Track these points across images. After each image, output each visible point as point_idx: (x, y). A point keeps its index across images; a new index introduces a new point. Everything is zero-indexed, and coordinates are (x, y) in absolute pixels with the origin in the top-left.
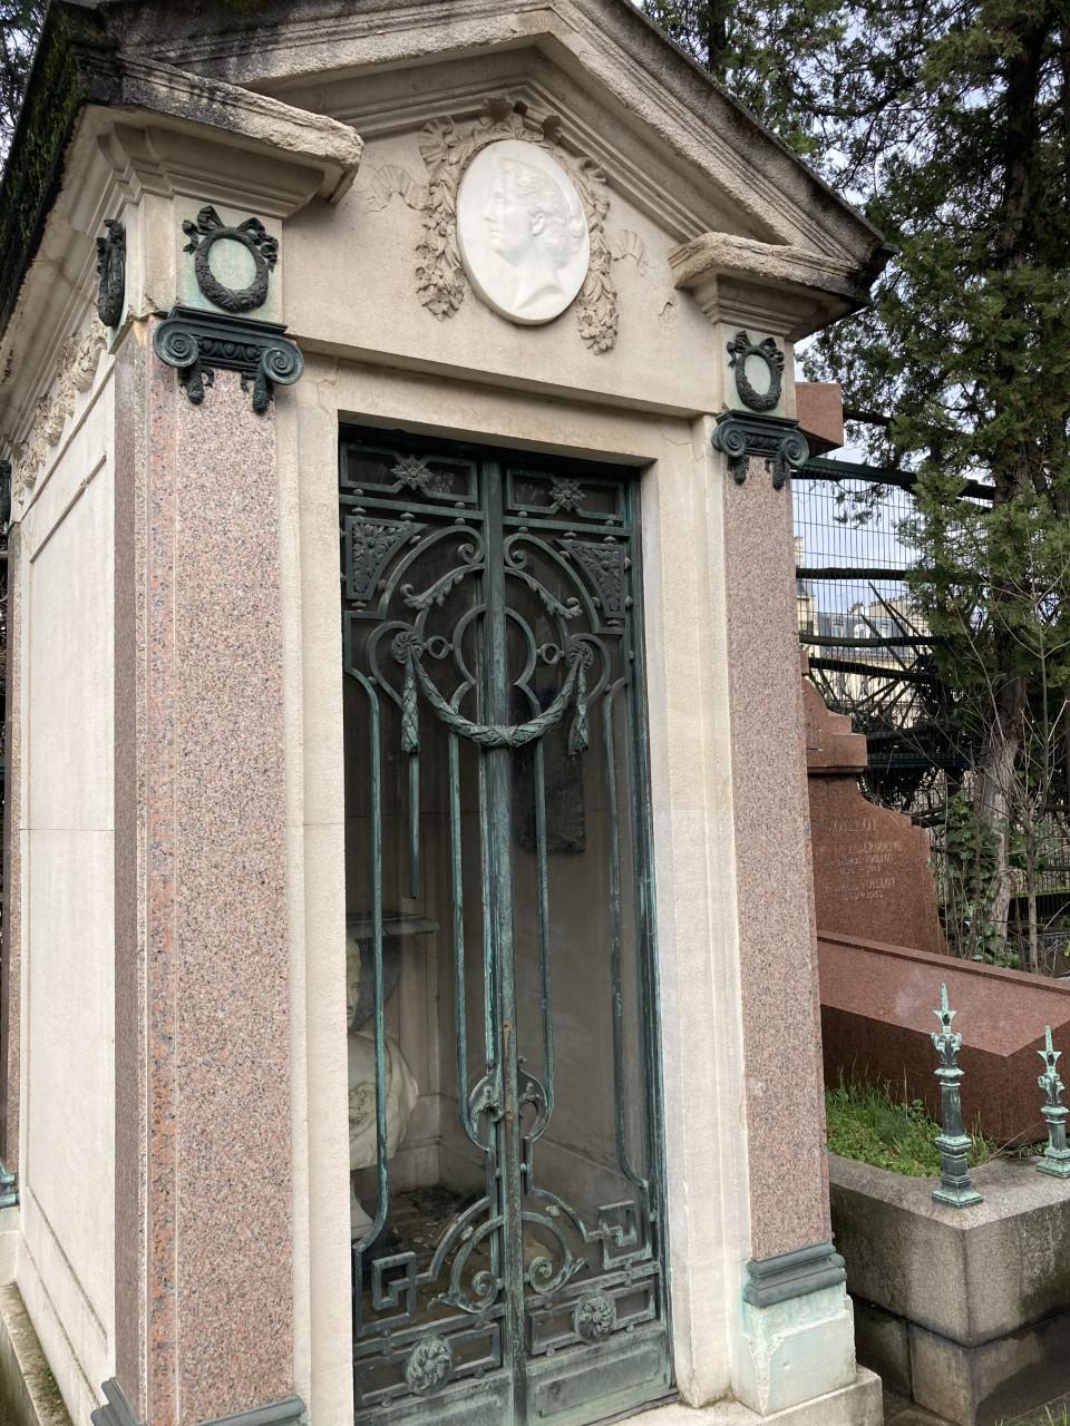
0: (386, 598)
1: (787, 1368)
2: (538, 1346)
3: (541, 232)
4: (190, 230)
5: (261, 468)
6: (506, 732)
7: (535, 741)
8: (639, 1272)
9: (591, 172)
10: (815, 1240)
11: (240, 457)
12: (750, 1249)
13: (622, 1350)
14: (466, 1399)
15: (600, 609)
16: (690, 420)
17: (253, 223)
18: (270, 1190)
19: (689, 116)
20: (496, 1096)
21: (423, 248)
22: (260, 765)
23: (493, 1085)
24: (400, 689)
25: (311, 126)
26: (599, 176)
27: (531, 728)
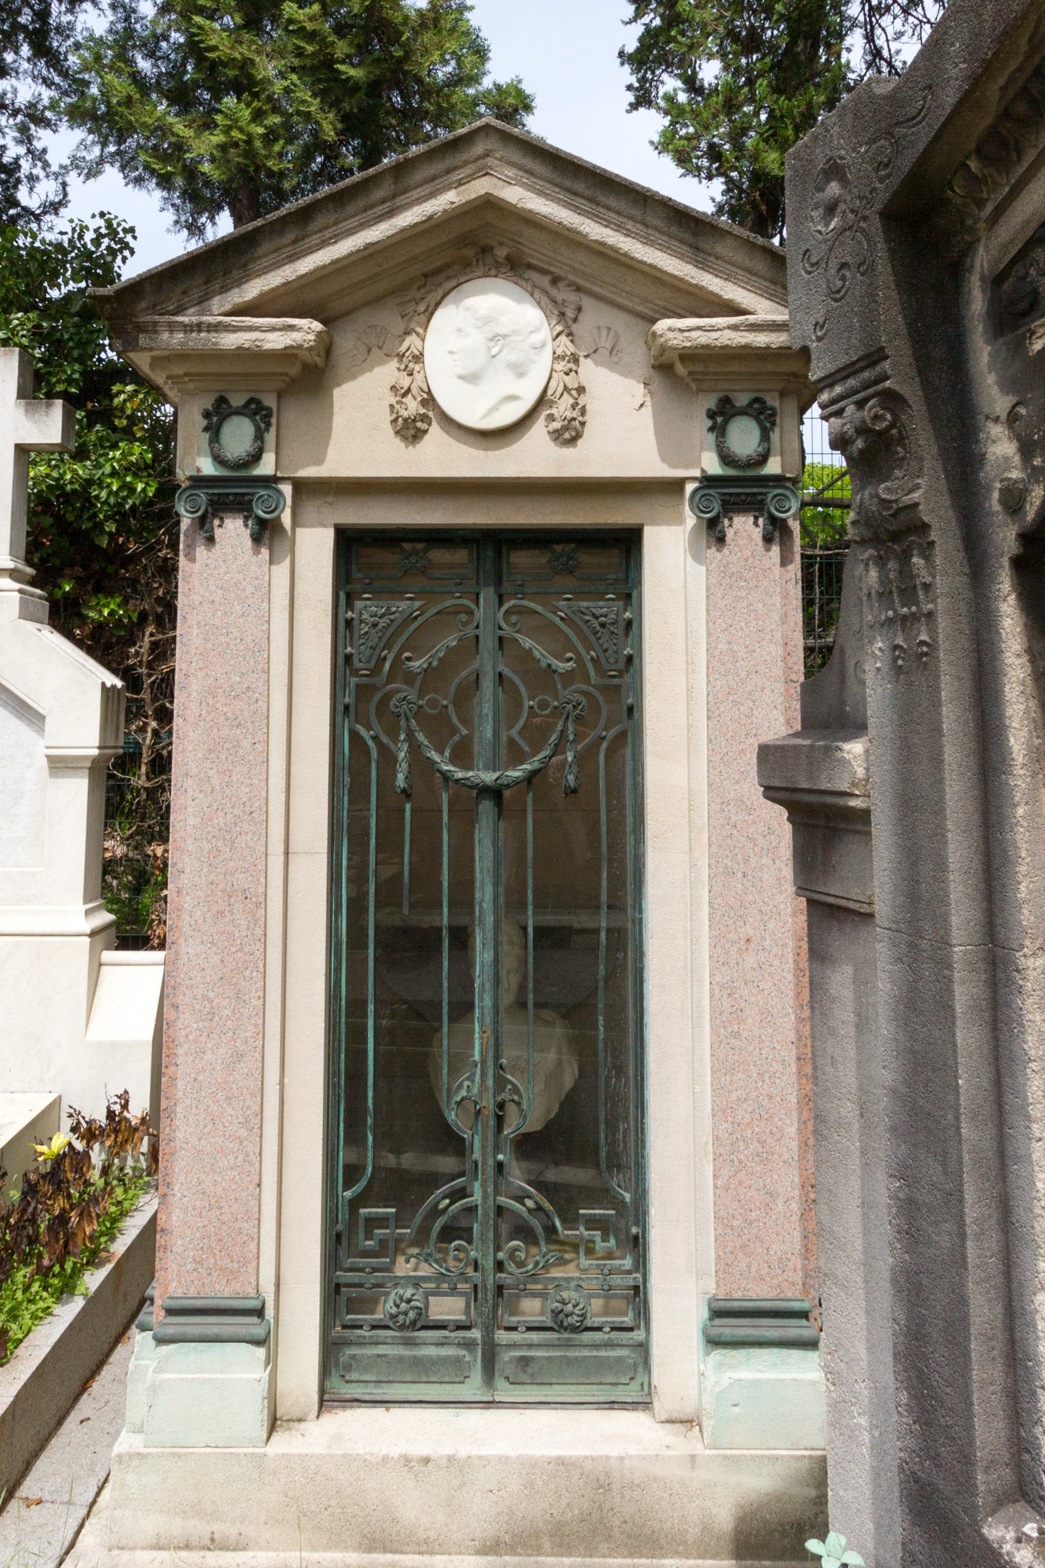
1: (736, 1409)
3: (500, 352)
4: (207, 415)
5: (256, 582)
9: (561, 285)
10: (789, 1295)
11: (241, 576)
12: (713, 1285)
13: (596, 1346)
14: (437, 1344)
16: (675, 486)
19: (630, 225)
20: (475, 1091)
22: (248, 809)
23: (473, 1081)
24: (396, 741)
25: (273, 329)
26: (569, 286)
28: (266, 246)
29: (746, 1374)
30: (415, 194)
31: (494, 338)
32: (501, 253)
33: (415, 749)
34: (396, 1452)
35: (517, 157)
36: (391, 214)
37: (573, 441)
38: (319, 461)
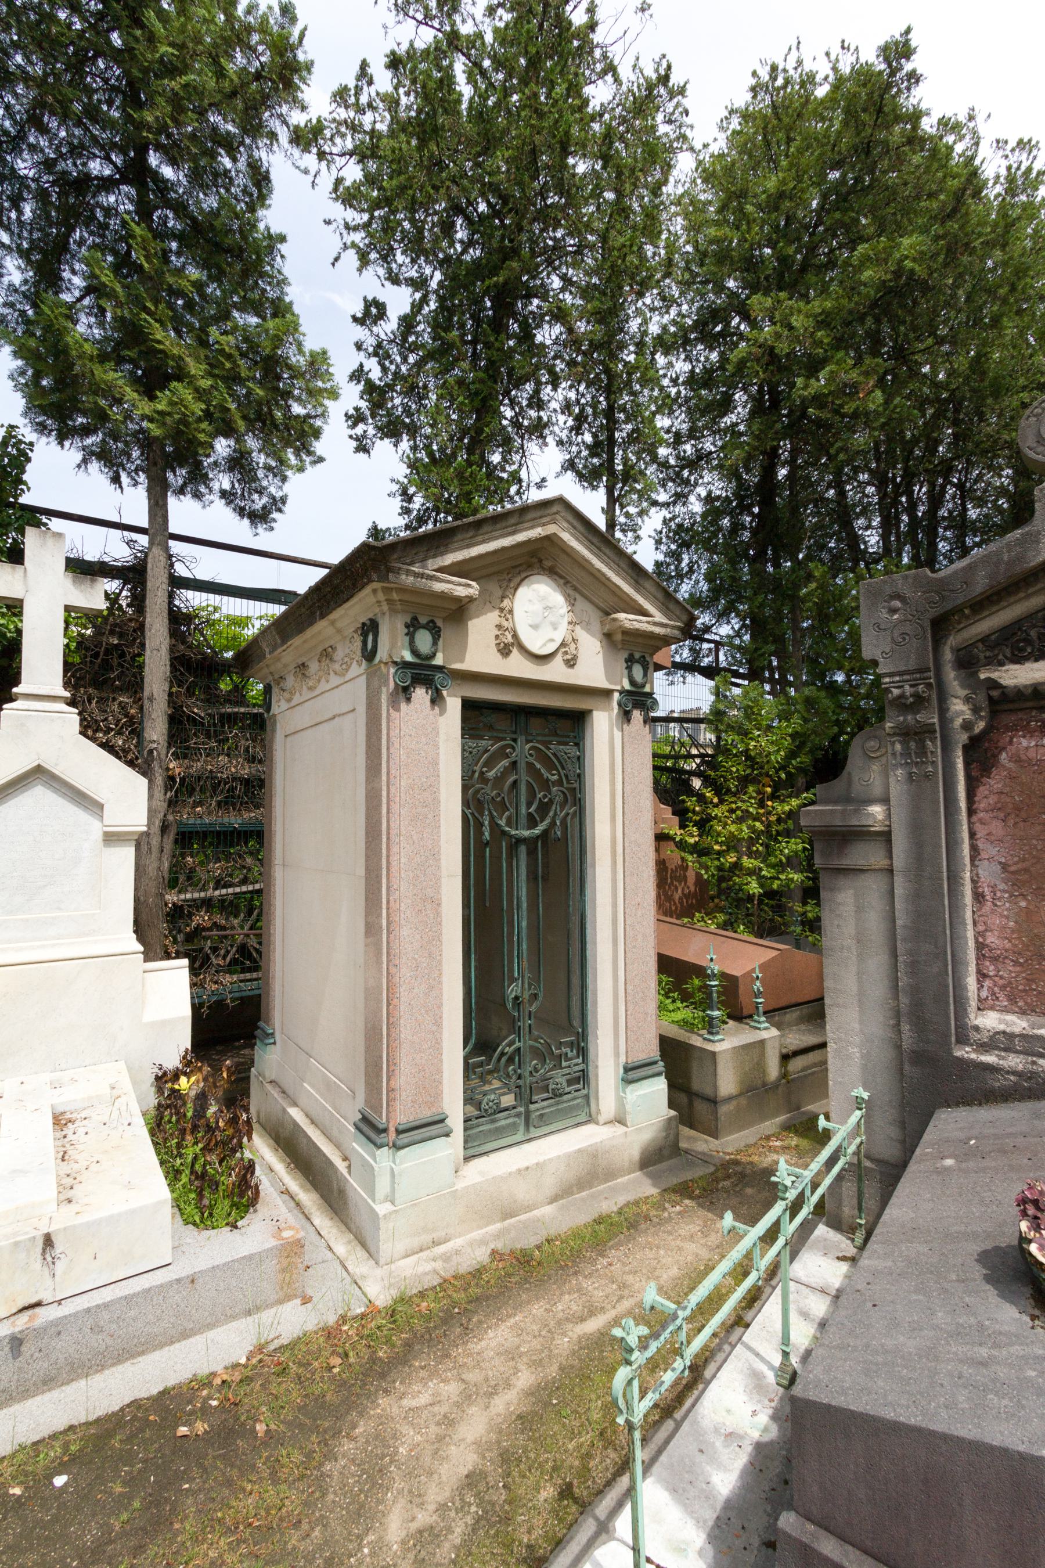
0: (477, 775)
2: (535, 1098)
4: (407, 626)
6: (526, 833)
7: (538, 837)
8: (577, 1068)
15: (566, 776)
16: (607, 693)
17: (432, 621)
18: (434, 1028)
21: (499, 627)
24: (482, 815)
25: (460, 585)
27: (537, 831)
28: (459, 537)
29: (641, 1092)
30: (526, 525)
31: (546, 608)
32: (547, 564)
33: (492, 817)
34: (514, 1169)
35: (570, 518)
36: (514, 533)
37: (572, 666)
38: (462, 661)
